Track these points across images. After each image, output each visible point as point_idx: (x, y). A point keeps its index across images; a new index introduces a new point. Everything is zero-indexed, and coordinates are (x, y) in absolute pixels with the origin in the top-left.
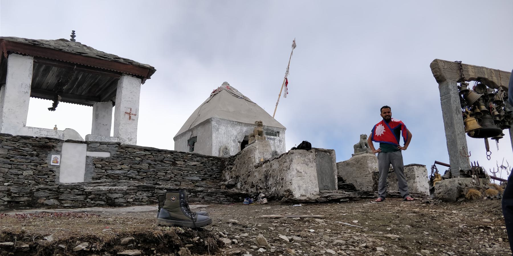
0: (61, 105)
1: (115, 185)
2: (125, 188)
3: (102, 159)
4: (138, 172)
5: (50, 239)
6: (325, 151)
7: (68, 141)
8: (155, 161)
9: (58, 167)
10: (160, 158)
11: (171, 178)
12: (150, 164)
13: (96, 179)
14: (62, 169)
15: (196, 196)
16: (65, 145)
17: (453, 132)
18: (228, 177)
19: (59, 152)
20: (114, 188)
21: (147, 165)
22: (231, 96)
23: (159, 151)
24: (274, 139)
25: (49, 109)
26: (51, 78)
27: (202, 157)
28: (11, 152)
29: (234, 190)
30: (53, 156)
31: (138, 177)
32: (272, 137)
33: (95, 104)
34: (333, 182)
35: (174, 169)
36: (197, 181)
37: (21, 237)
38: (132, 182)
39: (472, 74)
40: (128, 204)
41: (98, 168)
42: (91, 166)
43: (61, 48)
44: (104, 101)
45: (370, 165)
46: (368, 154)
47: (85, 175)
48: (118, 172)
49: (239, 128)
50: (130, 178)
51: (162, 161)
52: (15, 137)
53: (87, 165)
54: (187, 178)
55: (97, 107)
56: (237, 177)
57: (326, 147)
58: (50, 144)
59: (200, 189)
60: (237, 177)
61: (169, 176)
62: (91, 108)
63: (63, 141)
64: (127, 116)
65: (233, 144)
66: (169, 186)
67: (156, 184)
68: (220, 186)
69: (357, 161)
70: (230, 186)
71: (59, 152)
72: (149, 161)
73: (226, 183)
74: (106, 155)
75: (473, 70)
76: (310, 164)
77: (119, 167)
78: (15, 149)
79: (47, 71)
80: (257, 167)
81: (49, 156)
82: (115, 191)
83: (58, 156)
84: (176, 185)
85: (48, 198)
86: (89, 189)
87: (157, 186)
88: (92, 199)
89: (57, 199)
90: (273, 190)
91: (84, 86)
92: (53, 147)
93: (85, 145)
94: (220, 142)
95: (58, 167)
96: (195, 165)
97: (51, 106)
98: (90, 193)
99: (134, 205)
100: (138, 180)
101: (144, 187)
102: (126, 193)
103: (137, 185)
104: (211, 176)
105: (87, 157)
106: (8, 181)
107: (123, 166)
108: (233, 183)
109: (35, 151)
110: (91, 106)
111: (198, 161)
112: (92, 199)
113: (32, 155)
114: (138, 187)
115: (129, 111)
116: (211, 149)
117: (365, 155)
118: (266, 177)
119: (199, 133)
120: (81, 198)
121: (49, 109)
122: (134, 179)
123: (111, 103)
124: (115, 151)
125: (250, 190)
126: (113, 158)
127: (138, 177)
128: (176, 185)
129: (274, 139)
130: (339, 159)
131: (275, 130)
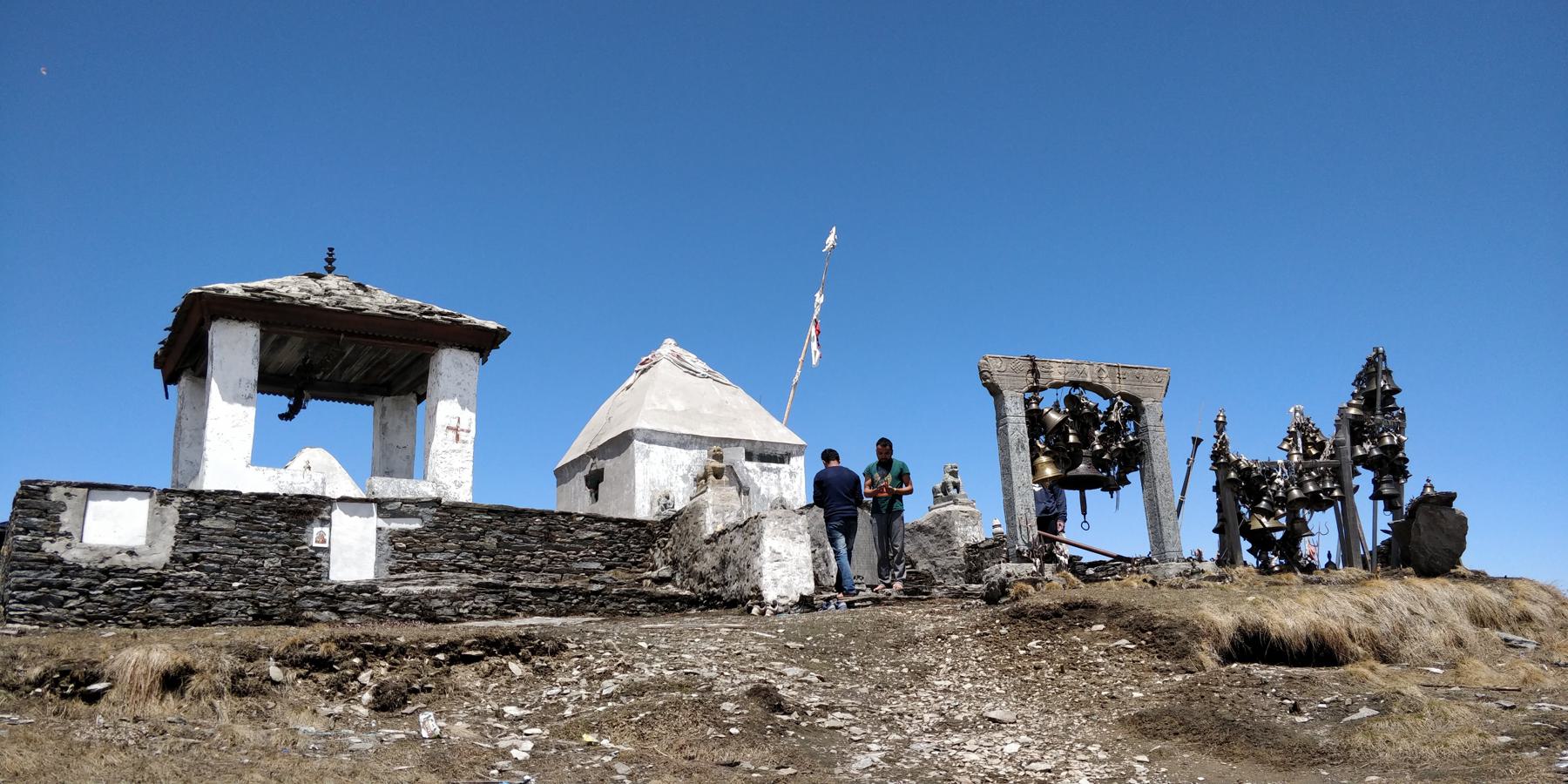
0: (315, 408)
1: (434, 584)
2: (454, 588)
3: (407, 533)
4: (478, 556)
5: (402, 640)
8: (511, 533)
9: (327, 550)
10: (520, 525)
12: (499, 539)
15: (588, 602)
19: (326, 522)
20: (434, 588)
22: (681, 371)
24: (778, 471)
25: (282, 417)
27: (608, 520)
30: (317, 530)
32: (774, 465)
33: (379, 401)
35: (546, 547)
36: (595, 572)
37: (378, 639)
38: (466, 576)
40: (460, 617)
41: (403, 552)
42: (386, 547)
44: (399, 394)
45: (960, 530)
46: (957, 507)
47: (377, 563)
48: (437, 556)
49: (695, 453)
50: (461, 568)
52: (247, 496)
53: (379, 546)
54: (576, 566)
55: (384, 409)
58: (310, 507)
59: (595, 587)
61: (539, 562)
62: (367, 411)
64: (452, 435)
65: (682, 485)
66: (538, 583)
67: (513, 579)
68: (640, 581)
70: (661, 581)
71: (326, 522)
72: (498, 533)
74: (414, 525)
76: (799, 537)
77: (440, 546)
79: (281, 342)
80: (708, 542)
81: (308, 529)
83: (326, 530)
84: (554, 580)
85: (318, 608)
86: (389, 591)
87: (514, 584)
88: (395, 610)
89: (334, 610)
90: (734, 587)
91: (355, 368)
92: (317, 512)
94: (652, 483)
96: (591, 538)
97: (285, 410)
98: (392, 599)
99: (470, 619)
100: (478, 572)
101: (488, 585)
102: (454, 598)
103: (476, 582)
104: (625, 559)
105: (379, 529)
106: (238, 580)
108: (668, 574)
109: (282, 520)
110: (368, 404)
111: (597, 530)
112: (395, 610)
113: (278, 529)
115: (454, 424)
116: (632, 497)
117: (950, 508)
118: (724, 562)
119: (608, 465)
120: (376, 607)
121: (282, 417)
122: (468, 569)
123: (412, 398)
124: (429, 513)
126: (428, 528)
127: (478, 566)
128: (554, 580)
129: (778, 471)
131: (781, 451)
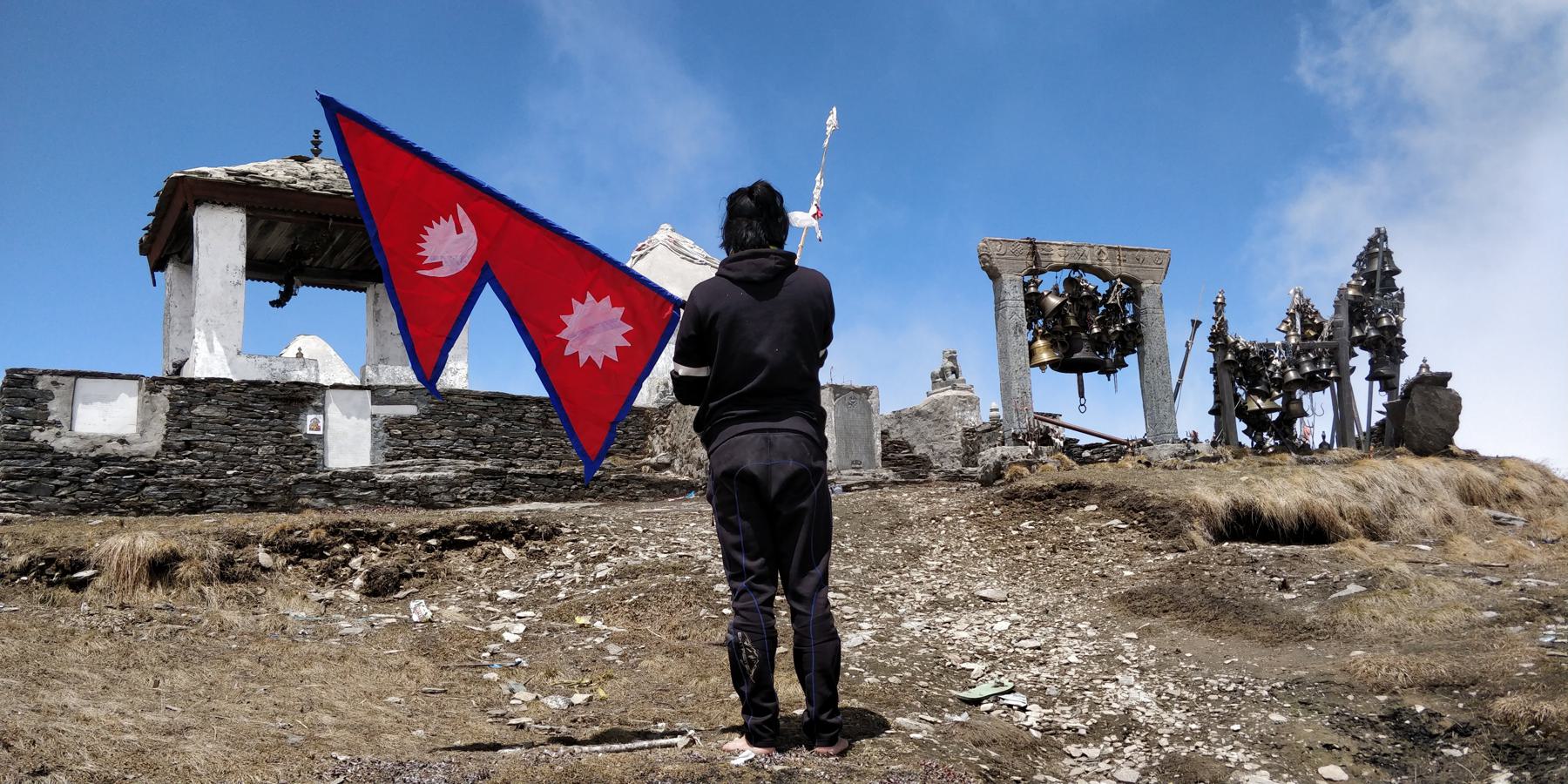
1: (431, 470)
2: (451, 474)
3: (401, 420)
4: (475, 442)
5: (393, 525)
6: (857, 391)
7: (336, 387)
8: (507, 419)
9: (321, 438)
11: (541, 452)
12: (496, 426)
13: (394, 458)
14: (330, 439)
15: (587, 487)
16: (330, 394)
17: (1008, 367)
18: (657, 449)
21: (492, 428)
22: (677, 258)
23: (515, 399)
25: (273, 304)
26: (278, 241)
28: (235, 412)
29: (669, 474)
31: (476, 453)
34: (871, 452)
39: (1057, 258)
42: (382, 434)
43: (299, 184)
48: (434, 443)
51: (520, 419)
53: (375, 434)
56: (674, 449)
57: (858, 384)
58: (302, 395)
60: (674, 449)
61: (537, 449)
62: (360, 297)
63: (324, 388)
67: (511, 465)
69: (936, 405)
70: (659, 467)
71: (320, 410)
72: (494, 420)
73: (653, 460)
75: (1062, 252)
77: (436, 433)
78: (240, 407)
82: (433, 482)
84: (552, 467)
86: (386, 477)
87: (512, 470)
91: (346, 253)
92: (310, 399)
93: (368, 393)
95: (321, 438)
97: (277, 297)
98: (388, 485)
100: (476, 459)
101: (486, 471)
104: (623, 446)
107: (444, 432)
108: (666, 460)
113: (272, 417)
114: (474, 472)
121: (273, 304)
122: (466, 456)
125: (696, 473)
127: (476, 453)
130: (887, 405)
